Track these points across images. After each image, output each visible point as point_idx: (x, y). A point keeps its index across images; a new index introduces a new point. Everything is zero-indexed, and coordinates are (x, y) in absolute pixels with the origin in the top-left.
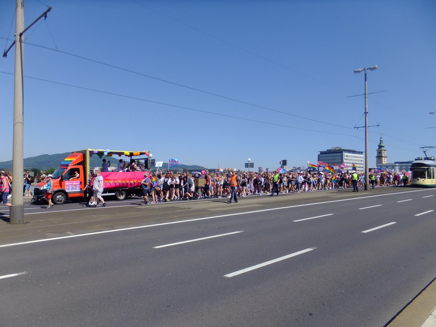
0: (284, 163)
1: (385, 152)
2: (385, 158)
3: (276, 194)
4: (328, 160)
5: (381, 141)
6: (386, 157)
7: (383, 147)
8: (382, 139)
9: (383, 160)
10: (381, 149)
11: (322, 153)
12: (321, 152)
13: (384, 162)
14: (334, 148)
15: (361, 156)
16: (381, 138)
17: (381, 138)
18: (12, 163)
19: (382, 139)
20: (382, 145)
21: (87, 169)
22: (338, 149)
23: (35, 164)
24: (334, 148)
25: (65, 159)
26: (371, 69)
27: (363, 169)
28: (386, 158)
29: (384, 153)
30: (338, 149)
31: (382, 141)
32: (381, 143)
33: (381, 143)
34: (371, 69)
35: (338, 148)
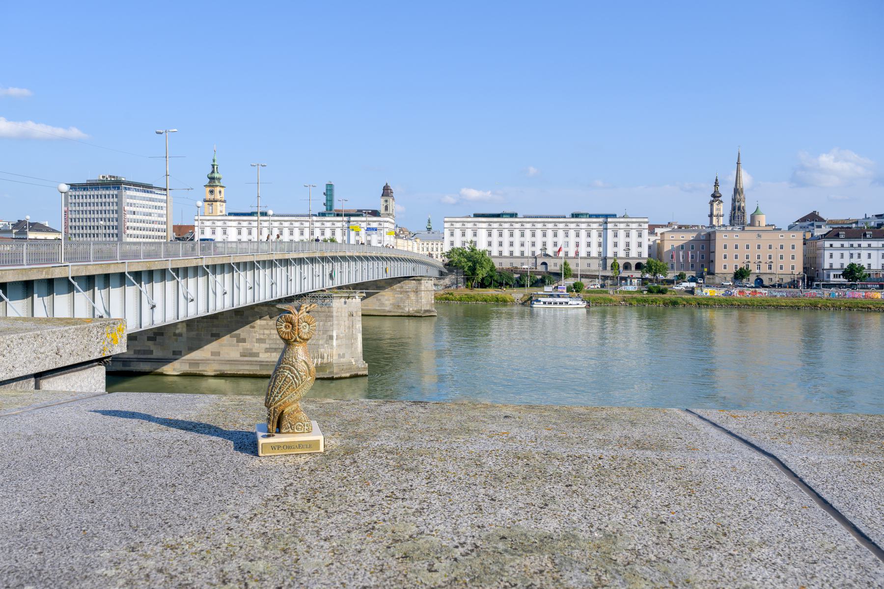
0: (345, 303)
1: (222, 190)
2: (222, 204)
4: (144, 230)
5: (213, 166)
6: (225, 201)
7: (219, 179)
10: (214, 184)
12: (71, 185)
14: (103, 177)
16: (214, 161)
17: (214, 161)
19: (216, 163)
20: (216, 175)
21: (66, 373)
22: (113, 179)
23: (656, 285)
24: (103, 177)
26: (262, 166)
27: (128, 201)
28: (224, 204)
29: (220, 192)
30: (113, 179)
31: (215, 167)
32: (213, 172)
33: (213, 172)
34: (262, 166)
35: (114, 177)
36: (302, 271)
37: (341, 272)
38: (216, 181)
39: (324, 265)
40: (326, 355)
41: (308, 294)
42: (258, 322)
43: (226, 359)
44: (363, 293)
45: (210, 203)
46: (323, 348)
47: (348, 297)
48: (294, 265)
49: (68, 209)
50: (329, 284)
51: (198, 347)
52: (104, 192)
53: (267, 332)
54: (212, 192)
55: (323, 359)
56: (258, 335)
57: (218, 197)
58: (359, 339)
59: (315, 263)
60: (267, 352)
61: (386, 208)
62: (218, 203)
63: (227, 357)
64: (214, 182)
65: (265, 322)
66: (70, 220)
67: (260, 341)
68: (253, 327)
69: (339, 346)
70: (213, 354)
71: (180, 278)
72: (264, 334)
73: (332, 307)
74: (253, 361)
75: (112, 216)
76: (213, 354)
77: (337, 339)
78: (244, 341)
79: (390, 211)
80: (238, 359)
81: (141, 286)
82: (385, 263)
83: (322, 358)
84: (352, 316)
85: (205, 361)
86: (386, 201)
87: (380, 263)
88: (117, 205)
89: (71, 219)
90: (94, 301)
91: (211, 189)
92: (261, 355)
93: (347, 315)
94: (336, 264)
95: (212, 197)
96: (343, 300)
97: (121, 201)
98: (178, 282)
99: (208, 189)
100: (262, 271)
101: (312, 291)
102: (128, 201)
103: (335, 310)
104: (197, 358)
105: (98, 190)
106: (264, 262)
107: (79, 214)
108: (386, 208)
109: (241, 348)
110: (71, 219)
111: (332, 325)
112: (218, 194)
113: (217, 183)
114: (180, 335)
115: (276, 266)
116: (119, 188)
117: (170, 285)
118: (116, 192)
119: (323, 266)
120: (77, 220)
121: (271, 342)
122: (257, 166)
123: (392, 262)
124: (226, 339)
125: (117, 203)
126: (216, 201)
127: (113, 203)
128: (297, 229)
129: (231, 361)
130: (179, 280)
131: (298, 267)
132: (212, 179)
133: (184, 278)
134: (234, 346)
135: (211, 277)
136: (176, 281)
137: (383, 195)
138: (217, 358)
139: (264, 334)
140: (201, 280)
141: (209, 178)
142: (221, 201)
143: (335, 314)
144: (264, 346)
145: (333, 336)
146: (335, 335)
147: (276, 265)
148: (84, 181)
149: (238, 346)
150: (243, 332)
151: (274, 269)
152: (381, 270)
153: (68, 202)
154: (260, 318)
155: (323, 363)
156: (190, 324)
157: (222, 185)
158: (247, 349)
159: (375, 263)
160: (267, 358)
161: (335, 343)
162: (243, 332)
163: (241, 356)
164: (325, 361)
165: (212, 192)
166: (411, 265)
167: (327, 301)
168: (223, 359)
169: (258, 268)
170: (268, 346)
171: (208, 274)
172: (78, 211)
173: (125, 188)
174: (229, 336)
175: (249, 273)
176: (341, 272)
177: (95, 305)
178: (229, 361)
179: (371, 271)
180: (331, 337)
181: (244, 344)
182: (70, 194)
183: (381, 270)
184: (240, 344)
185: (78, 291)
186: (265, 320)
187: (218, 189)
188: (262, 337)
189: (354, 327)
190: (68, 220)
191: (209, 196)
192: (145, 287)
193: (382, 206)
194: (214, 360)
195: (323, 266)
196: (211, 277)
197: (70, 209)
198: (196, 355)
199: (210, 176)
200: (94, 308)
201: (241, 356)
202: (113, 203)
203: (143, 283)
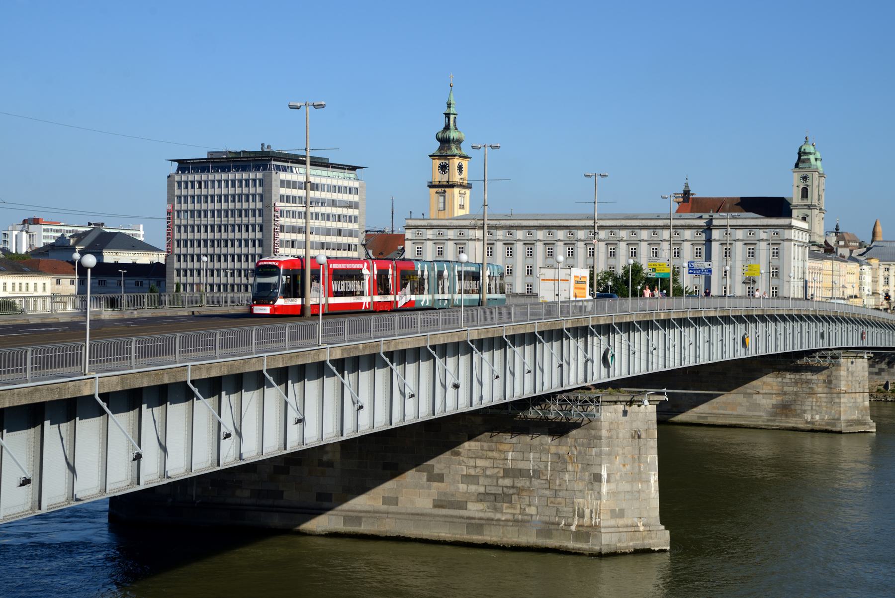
0: (625, 413)
1: (465, 163)
2: (463, 191)
3: (73, 289)
5: (448, 115)
6: (469, 187)
7: (458, 142)
8: (452, 110)
9: (457, 201)
10: (449, 153)
11: (184, 166)
12: (179, 161)
13: (462, 207)
15: (679, 315)
18: (66, 512)
19: (452, 110)
20: (453, 134)
25: (299, 525)
27: (284, 191)
28: (468, 192)
29: (460, 168)
31: (452, 117)
33: (447, 128)
36: (650, 338)
37: (808, 332)
38: (453, 147)
39: (394, 367)
40: (587, 513)
41: (554, 395)
42: (468, 446)
43: (409, 511)
44: (662, 394)
45: (440, 190)
46: (583, 498)
47: (631, 403)
48: (618, 333)
49: (173, 207)
50: (599, 375)
51: (362, 490)
52: (238, 176)
53: (480, 463)
54: (444, 168)
55: (583, 517)
56: (464, 468)
57: (456, 178)
58: (652, 482)
59: (669, 328)
60: (481, 501)
61: (805, 193)
62: (456, 190)
63: (410, 508)
64: (449, 148)
65: (478, 444)
66: (176, 229)
67: (468, 479)
68: (458, 454)
69: (613, 494)
70: (386, 501)
71: (395, 364)
72: (476, 467)
73: (599, 420)
74: (456, 517)
75: (252, 220)
76: (386, 501)
77: (608, 481)
78: (440, 478)
79: (813, 198)
80: (428, 511)
81: (343, 377)
82: (819, 325)
83: (581, 516)
84: (639, 437)
85: (374, 514)
86: (805, 178)
87: (812, 325)
88: (261, 200)
89: (179, 256)
90: (220, 414)
91: (443, 161)
92: (470, 506)
93: (628, 435)
94: (715, 328)
95: (444, 178)
96: (620, 407)
97: (270, 191)
98: (392, 370)
99: (438, 162)
100: (572, 341)
101: (561, 389)
102: (284, 191)
103: (605, 424)
104: (359, 508)
105: (229, 171)
106: (444, 346)
107: (192, 216)
108: (805, 193)
109: (433, 491)
110: (179, 256)
111: (599, 455)
112: (457, 171)
113: (454, 150)
114: (330, 464)
115: (614, 331)
116: (265, 169)
117: (381, 374)
118: (259, 175)
119: (681, 332)
120: (197, 185)
121: (487, 481)
122: (483, 149)
123: (826, 324)
124: (411, 476)
125: (261, 196)
126: (452, 186)
127: (254, 196)
128: (560, 244)
129: (418, 514)
130: (394, 367)
131: (625, 336)
132: (445, 142)
133: (399, 364)
134: (422, 487)
135: (439, 362)
136: (388, 368)
137: (797, 166)
138: (392, 508)
139: (476, 467)
140: (464, 360)
141: (439, 140)
142: (461, 186)
143: (604, 433)
144: (473, 488)
145: (601, 475)
146: (604, 473)
147: (592, 334)
148: (202, 154)
149: (429, 488)
150: (439, 463)
151: (565, 342)
152: (813, 335)
153: (173, 195)
154: (470, 438)
155: (582, 526)
156: (350, 447)
157: (464, 152)
158: (445, 494)
159: (804, 324)
160: (482, 511)
161: (605, 488)
162: (438, 462)
163: (435, 506)
164: (587, 520)
165: (444, 168)
166: (815, 328)
167: (592, 407)
168: (403, 511)
169: (568, 338)
170: (482, 490)
171: (472, 350)
172: (192, 212)
173: (278, 168)
174: (415, 469)
175: (602, 338)
176: (808, 332)
177: (222, 420)
178: (412, 514)
179: (772, 340)
180: (598, 478)
181: (440, 484)
182: (177, 178)
183: (813, 335)
184: (435, 484)
185: (198, 399)
186: (478, 441)
187: (456, 162)
188: (472, 472)
189: (643, 459)
190: (173, 230)
191: (439, 177)
192: (349, 378)
193: (795, 188)
194: (388, 513)
195: (681, 332)
196: (439, 362)
197: (177, 207)
198: (360, 502)
199: (440, 135)
200: (219, 424)
201: (435, 506)
202: (254, 196)
203: (346, 372)
